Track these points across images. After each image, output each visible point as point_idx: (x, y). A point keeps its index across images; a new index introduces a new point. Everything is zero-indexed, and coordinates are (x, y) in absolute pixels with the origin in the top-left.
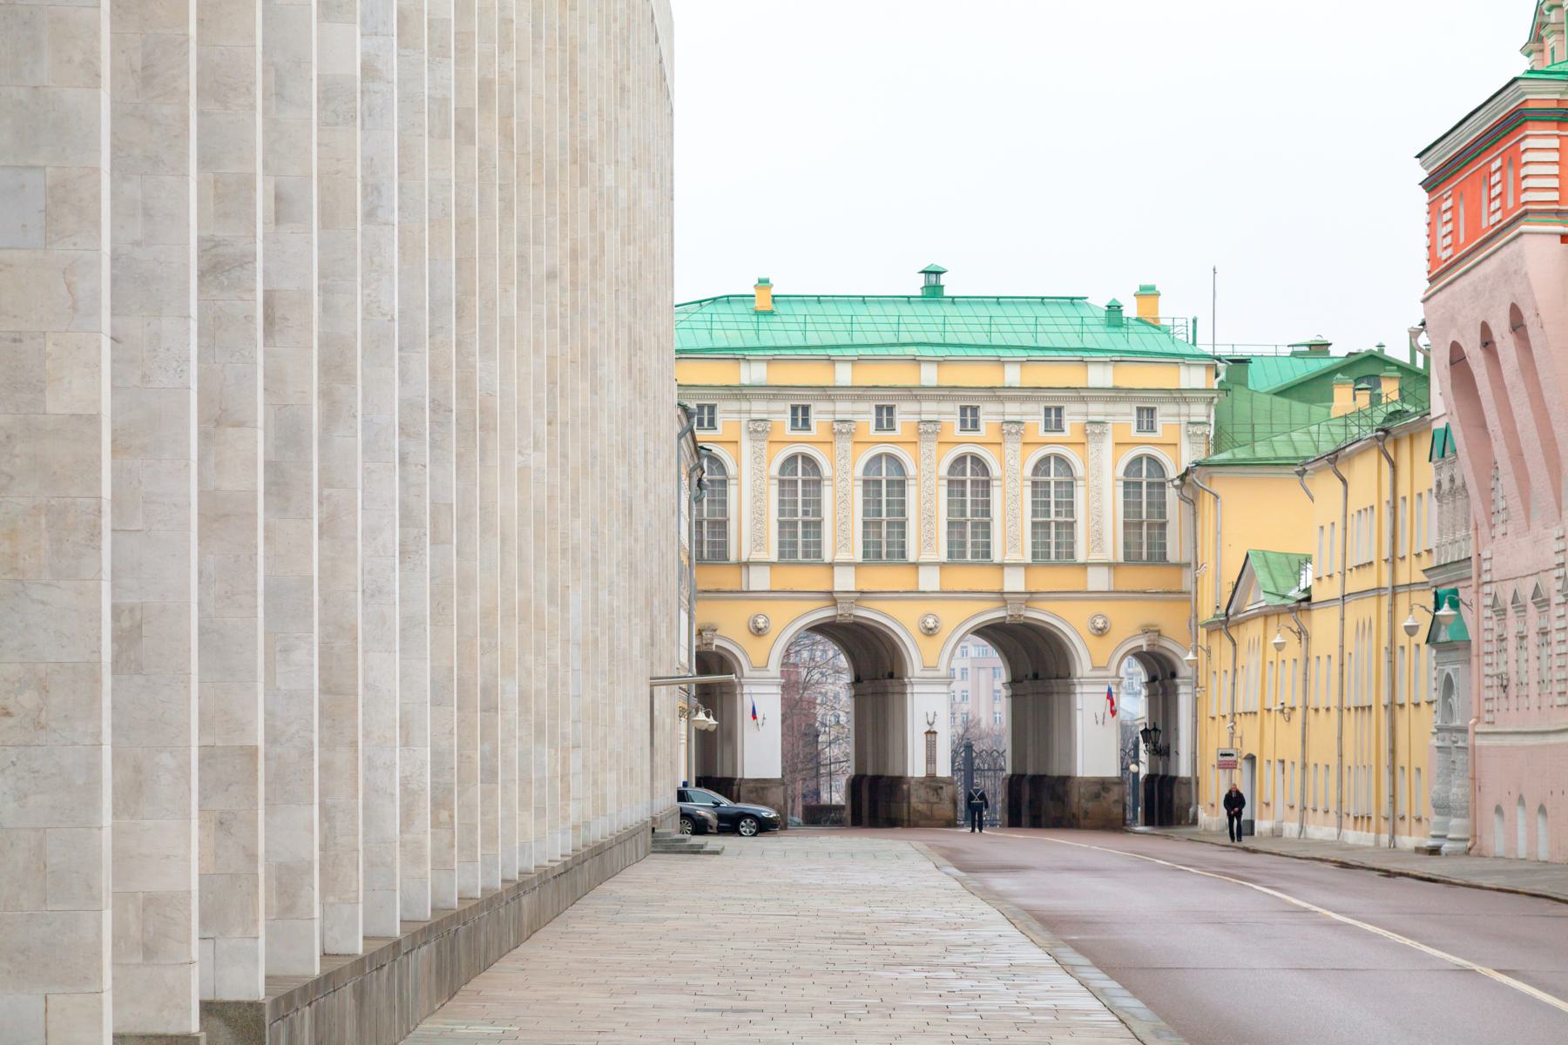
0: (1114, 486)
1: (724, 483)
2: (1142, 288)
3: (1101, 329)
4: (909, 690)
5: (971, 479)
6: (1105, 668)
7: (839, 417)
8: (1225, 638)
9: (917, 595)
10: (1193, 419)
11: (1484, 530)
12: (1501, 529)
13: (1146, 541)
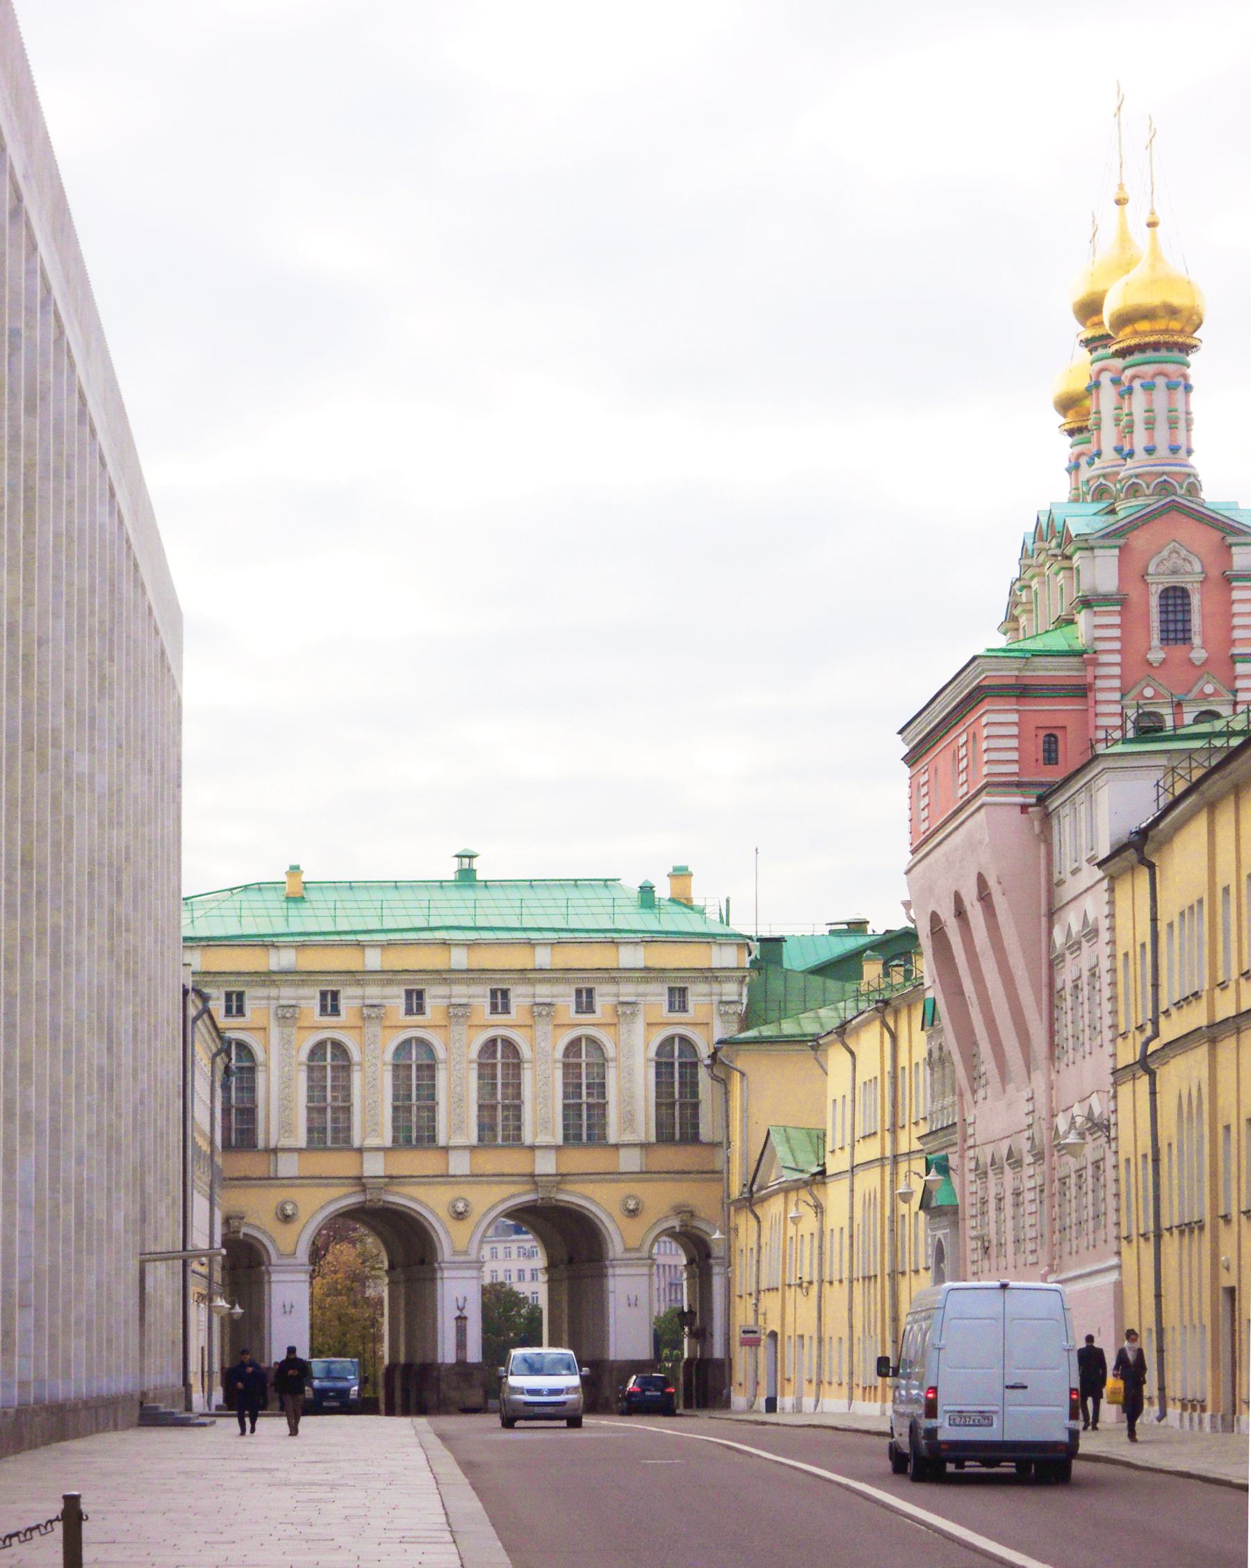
0: (646, 1067)
1: (252, 1070)
2: (675, 869)
3: (632, 910)
4: (439, 1275)
5: (501, 1062)
6: (638, 1250)
7: (368, 1002)
8: (751, 1216)
9: (445, 1178)
10: (725, 998)
11: (968, 1096)
12: (981, 1093)
13: (679, 1121)
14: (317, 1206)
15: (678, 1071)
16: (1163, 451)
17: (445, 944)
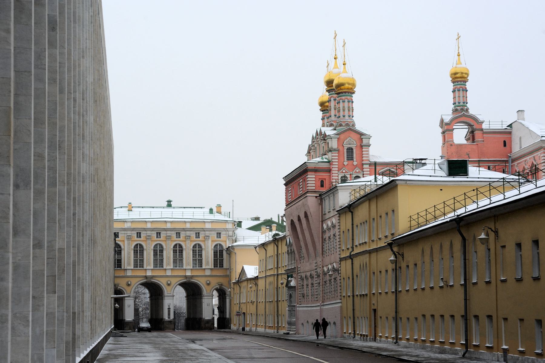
12: (302, 261)
16: (342, 117)
17: (166, 222)
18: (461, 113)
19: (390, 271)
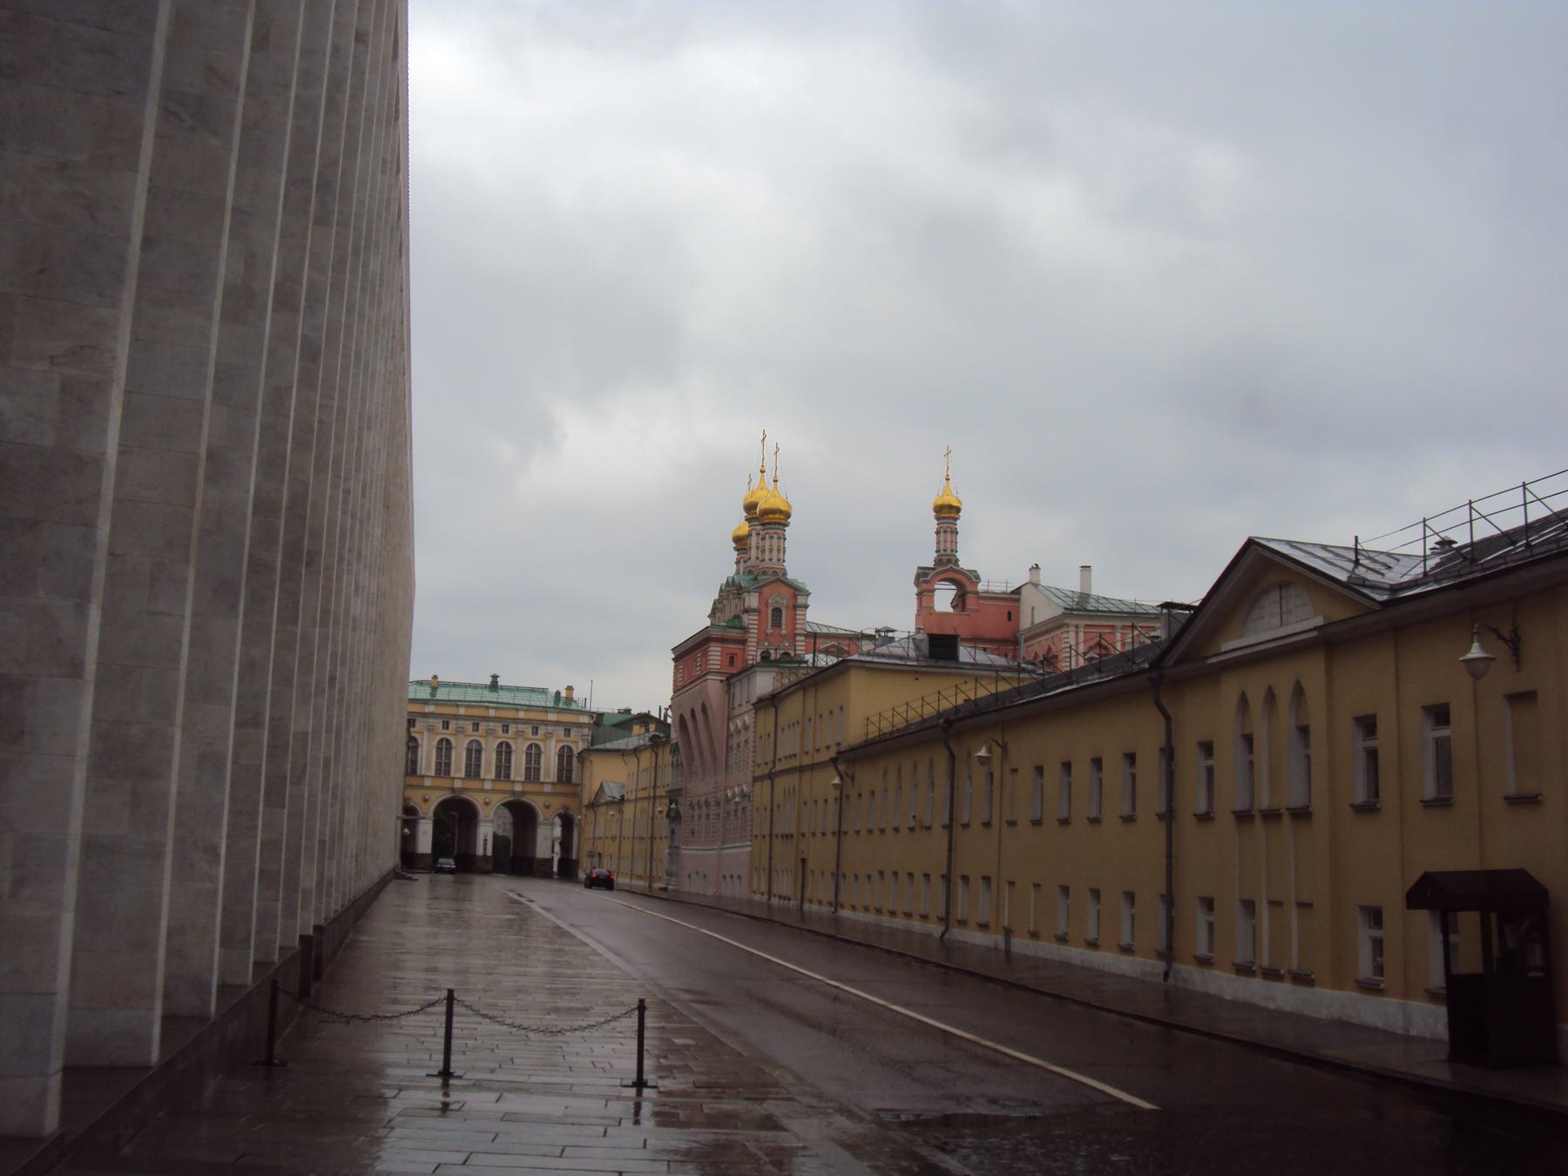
5: (505, 751)
9: (483, 790)
13: (565, 774)
14: (437, 798)
15: (565, 755)
18: (946, 568)
19: (831, 801)
